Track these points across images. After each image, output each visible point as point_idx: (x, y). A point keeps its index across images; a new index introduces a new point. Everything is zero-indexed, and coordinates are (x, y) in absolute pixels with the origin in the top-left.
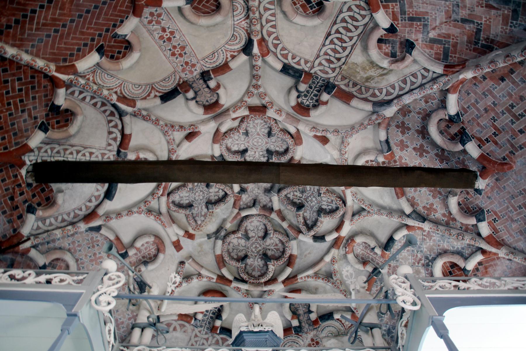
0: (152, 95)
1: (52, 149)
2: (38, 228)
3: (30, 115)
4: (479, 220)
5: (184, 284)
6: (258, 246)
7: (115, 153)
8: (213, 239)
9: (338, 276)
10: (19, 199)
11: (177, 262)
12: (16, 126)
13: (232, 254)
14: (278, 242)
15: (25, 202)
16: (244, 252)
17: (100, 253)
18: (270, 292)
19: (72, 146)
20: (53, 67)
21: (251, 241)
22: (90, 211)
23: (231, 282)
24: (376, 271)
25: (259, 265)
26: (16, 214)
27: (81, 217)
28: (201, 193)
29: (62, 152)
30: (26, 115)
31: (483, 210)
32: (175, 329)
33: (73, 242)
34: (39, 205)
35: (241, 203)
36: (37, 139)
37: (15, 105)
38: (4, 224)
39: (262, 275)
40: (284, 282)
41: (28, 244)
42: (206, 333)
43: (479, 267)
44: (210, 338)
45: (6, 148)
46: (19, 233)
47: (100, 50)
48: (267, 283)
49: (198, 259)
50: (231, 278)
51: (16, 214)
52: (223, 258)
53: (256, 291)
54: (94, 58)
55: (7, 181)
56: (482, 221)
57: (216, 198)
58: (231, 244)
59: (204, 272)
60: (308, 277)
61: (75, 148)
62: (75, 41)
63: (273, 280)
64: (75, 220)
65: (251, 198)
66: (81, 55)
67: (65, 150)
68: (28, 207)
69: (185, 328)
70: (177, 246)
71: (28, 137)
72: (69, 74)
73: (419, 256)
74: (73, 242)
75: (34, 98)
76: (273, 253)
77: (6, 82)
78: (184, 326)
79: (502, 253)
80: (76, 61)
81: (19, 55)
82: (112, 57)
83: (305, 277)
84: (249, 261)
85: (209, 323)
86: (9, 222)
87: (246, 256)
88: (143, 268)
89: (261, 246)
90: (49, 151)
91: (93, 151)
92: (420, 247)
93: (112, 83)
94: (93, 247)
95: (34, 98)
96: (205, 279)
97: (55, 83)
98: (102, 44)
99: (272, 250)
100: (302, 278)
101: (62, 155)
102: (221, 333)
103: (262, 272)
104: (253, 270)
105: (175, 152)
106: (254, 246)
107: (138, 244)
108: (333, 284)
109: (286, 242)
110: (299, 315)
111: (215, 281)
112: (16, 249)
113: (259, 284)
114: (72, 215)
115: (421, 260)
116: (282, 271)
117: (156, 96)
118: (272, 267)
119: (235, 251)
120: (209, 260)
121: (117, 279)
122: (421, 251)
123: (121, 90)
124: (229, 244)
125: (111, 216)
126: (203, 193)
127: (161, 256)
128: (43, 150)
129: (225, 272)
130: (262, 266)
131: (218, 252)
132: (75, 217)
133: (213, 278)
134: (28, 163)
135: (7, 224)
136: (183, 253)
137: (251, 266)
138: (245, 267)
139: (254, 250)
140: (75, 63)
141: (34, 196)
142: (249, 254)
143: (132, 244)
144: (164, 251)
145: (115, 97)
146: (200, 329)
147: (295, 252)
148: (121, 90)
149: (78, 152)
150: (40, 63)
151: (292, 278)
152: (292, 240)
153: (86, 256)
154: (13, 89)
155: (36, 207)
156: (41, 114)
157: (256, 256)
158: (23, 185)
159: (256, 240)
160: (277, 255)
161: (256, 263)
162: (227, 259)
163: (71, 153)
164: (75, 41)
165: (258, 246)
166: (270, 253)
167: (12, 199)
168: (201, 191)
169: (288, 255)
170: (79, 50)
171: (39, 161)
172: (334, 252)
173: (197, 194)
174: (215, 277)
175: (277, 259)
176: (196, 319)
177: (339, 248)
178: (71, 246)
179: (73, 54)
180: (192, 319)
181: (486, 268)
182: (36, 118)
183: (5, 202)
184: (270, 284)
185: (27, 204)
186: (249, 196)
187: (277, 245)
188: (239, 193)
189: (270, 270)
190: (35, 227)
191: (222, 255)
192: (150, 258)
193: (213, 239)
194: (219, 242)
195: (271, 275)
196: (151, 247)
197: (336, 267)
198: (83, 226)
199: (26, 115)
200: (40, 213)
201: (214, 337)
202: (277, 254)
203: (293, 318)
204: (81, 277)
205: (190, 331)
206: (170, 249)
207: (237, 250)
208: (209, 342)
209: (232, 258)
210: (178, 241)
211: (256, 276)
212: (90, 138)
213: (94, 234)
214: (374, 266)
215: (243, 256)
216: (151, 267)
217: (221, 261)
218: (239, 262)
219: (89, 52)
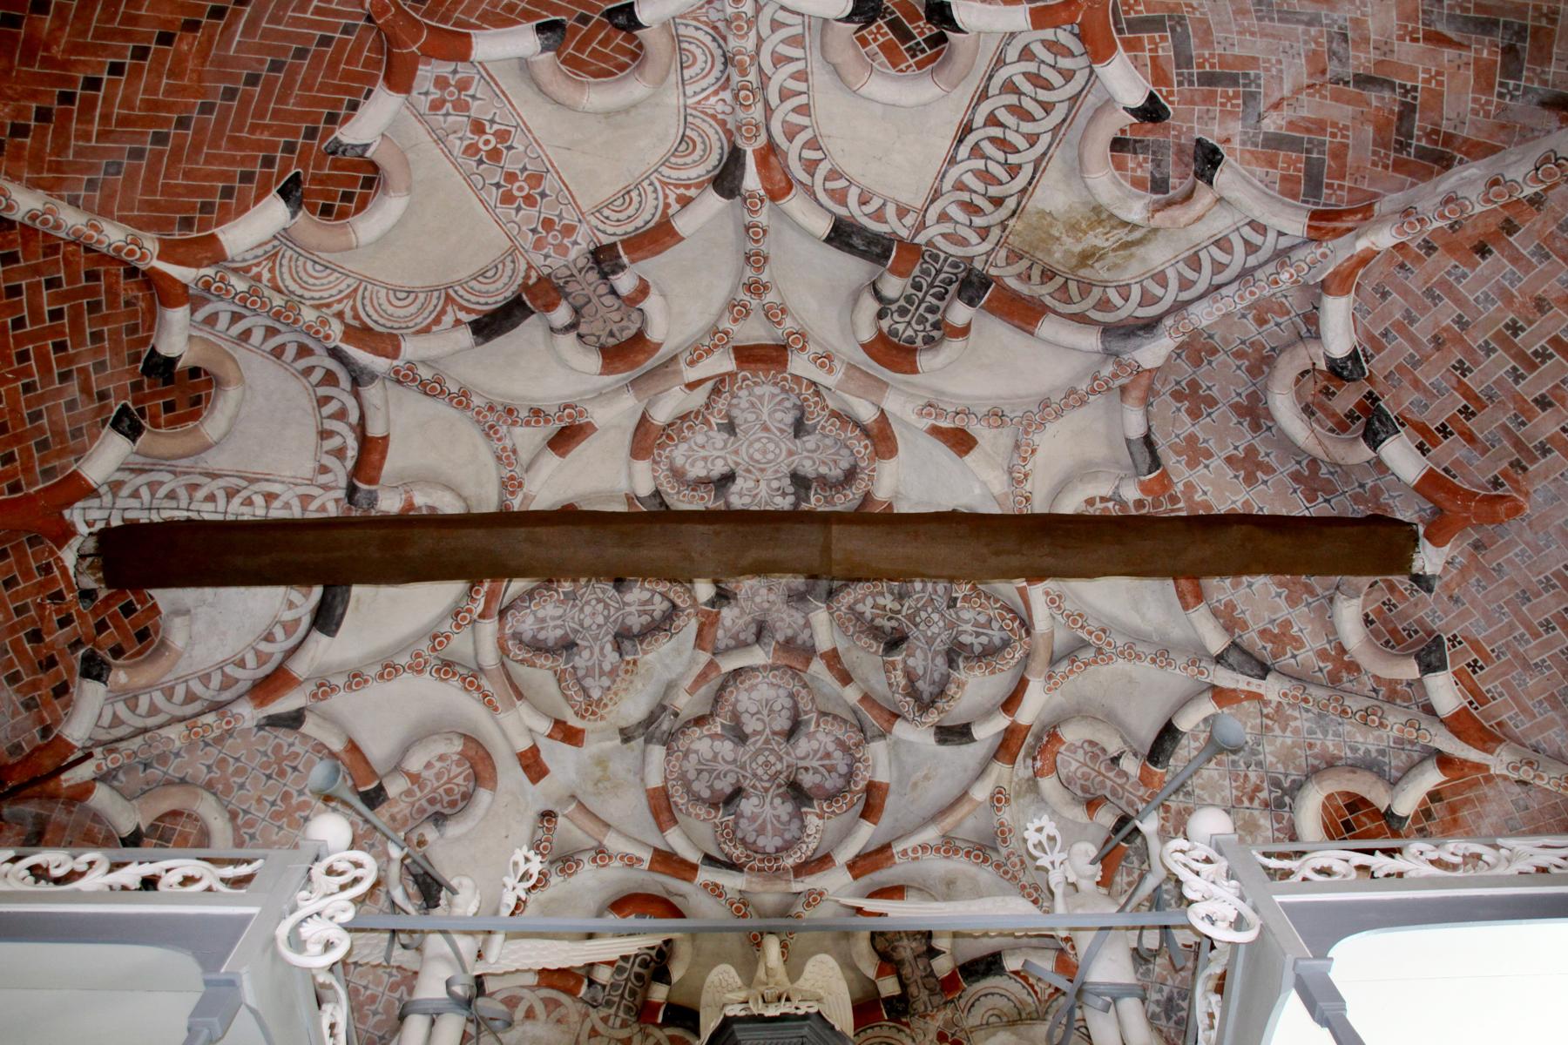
1: (153, 486)
6: (772, 759)
12: (45, 421)
13: (696, 786)
14: (831, 747)
16: (731, 779)
19: (214, 476)
20: (151, 243)
22: (268, 669)
26: (48, 680)
30: (74, 387)
32: (530, 1014)
33: (222, 762)
34: (117, 652)
38: (15, 714)
41: (85, 772)
42: (624, 1025)
49: (593, 804)
50: (694, 857)
51: (48, 680)
52: (668, 797)
54: (272, 214)
59: (613, 843)
61: (221, 482)
64: (226, 696)
65: (748, 618)
66: (234, 204)
68: (85, 659)
69: (562, 1010)
71: (80, 453)
74: (222, 762)
75: (97, 337)
76: (817, 779)
80: (219, 224)
83: (915, 850)
84: (747, 806)
85: (633, 993)
86: (27, 707)
87: (738, 792)
91: (275, 488)
92: (1254, 753)
94: (282, 773)
98: (297, 174)
99: (816, 771)
104: (761, 831)
106: (761, 759)
109: (857, 745)
110: (901, 963)
113: (778, 873)
114: (216, 680)
115: (1258, 789)
116: (846, 833)
117: (458, 322)
119: (705, 775)
122: (1259, 764)
123: (354, 308)
124: (686, 755)
130: (785, 818)
131: (655, 781)
132: (224, 687)
133: (640, 860)
134: (83, 529)
135: (25, 714)
137: (753, 819)
139: (760, 771)
140: (216, 231)
142: (746, 784)
145: (336, 329)
147: (882, 776)
148: (354, 308)
149: (231, 494)
152: (873, 738)
153: (260, 800)
155: (109, 658)
156: (117, 381)
157: (767, 790)
158: (69, 597)
159: (767, 742)
160: (829, 784)
162: (679, 799)
163: (211, 498)
165: (772, 759)
166: (807, 780)
167: (36, 636)
168: (599, 601)
169: (862, 785)
170: (227, 192)
173: (588, 610)
176: (592, 983)
182: (103, 396)
183: (16, 646)
184: (811, 873)
185: (81, 652)
186: (743, 611)
187: (828, 755)
188: (712, 603)
189: (811, 830)
190: (106, 720)
191: (664, 789)
196: (455, 770)
199: (74, 387)
201: (647, 1036)
202: (832, 783)
207: (710, 772)
210: (535, 750)
211: (770, 849)
213: (284, 736)
214: (1119, 812)
215: (728, 790)
219: (258, 199)
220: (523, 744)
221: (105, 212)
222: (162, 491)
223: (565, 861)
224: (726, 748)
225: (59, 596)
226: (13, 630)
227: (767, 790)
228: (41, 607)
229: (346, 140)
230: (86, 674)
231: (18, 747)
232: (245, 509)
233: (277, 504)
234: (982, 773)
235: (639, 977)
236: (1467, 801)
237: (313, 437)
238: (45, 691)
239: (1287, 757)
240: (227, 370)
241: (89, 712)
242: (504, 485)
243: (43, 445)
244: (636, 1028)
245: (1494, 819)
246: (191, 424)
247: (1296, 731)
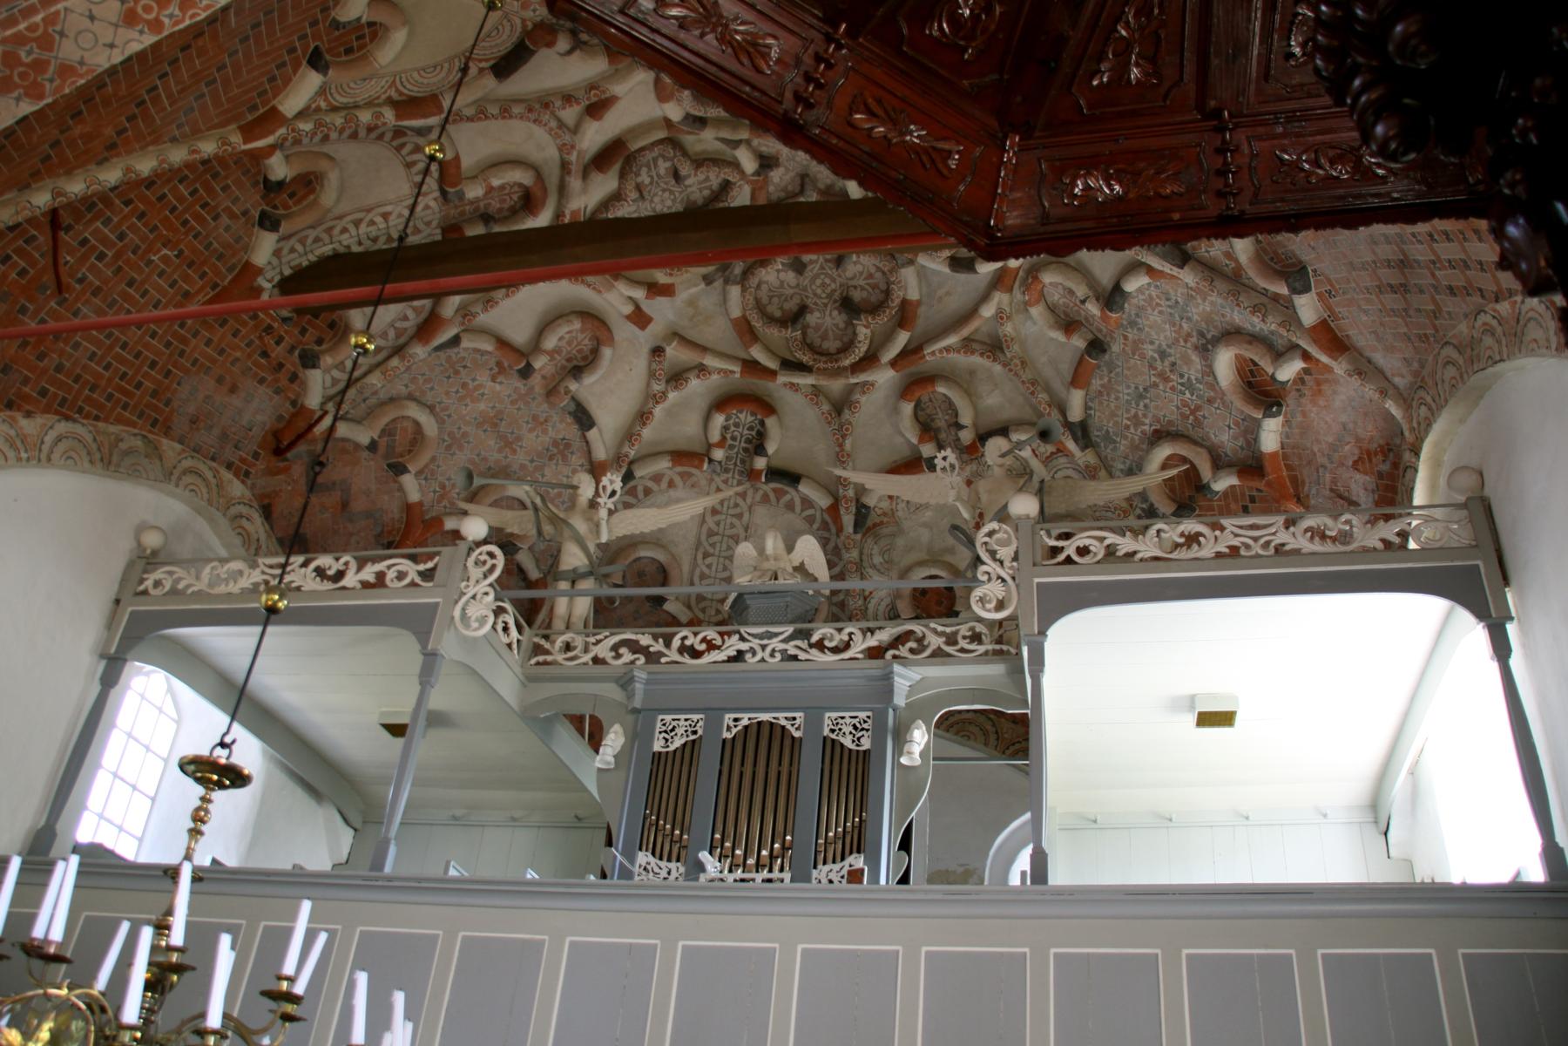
0: (473, 70)
1: (302, 242)
2: (335, 381)
3: (232, 216)
4: (1295, 291)
5: (672, 395)
6: (827, 281)
7: (437, 194)
8: (718, 284)
9: (1016, 347)
10: (278, 352)
11: (645, 351)
12: (215, 245)
13: (770, 309)
14: (873, 270)
15: (292, 350)
16: (796, 300)
17: (474, 380)
18: (866, 387)
19: (340, 218)
20: (236, 139)
21: (808, 273)
22: (424, 315)
23: (772, 374)
24: (1097, 347)
25: (836, 325)
26: (283, 378)
27: (410, 332)
28: (666, 194)
29: (325, 237)
30: (225, 220)
31: (1304, 268)
32: (671, 484)
33: (414, 380)
34: (319, 342)
35: (771, 189)
36: (264, 250)
37: (198, 218)
38: (271, 399)
39: (847, 348)
40: (894, 363)
41: (327, 422)
42: (740, 483)
43: (1306, 378)
44: (750, 493)
45: (215, 286)
46: (303, 406)
47: (317, 61)
48: (857, 368)
49: (692, 334)
50: (772, 364)
51: (283, 378)
52: (748, 323)
53: (836, 385)
54: (310, 82)
55: (244, 331)
56: (1300, 293)
57: (706, 193)
58: (764, 287)
59: (710, 361)
60: (948, 349)
61: (349, 218)
62: (256, 73)
63: (870, 360)
64: (402, 341)
65: (792, 174)
66: (280, 82)
67: (329, 230)
68: (301, 357)
69: (694, 479)
70: (640, 318)
71: (246, 248)
72: (273, 132)
73: (1185, 326)
74: (414, 380)
75: (225, 188)
76: (865, 294)
77: (164, 196)
78: (690, 475)
79: (1340, 367)
80: (275, 97)
81: (163, 161)
82: (348, 51)
83: (941, 351)
84: (812, 319)
85: (743, 462)
86: (277, 393)
87: (803, 310)
88: (573, 386)
89: (834, 280)
90: (299, 248)
91: (389, 208)
92: (1184, 311)
93: (375, 88)
94: (457, 373)
95: (225, 188)
96: (715, 377)
97: (258, 157)
98: (317, 48)
99: (863, 289)
100: (933, 353)
101: (327, 240)
102: (768, 481)
103: (846, 339)
104: (824, 337)
105: (573, 147)
106: (818, 282)
107: (550, 342)
108: (1005, 365)
109: (891, 271)
110: (938, 430)
111: (738, 375)
112: (310, 436)
113: (838, 372)
114: (392, 334)
115: (1189, 335)
116: (888, 337)
117: (481, 70)
118: (864, 332)
119: (775, 300)
120: (717, 331)
121: (490, 562)
122: (1189, 319)
123: (397, 90)
124: (758, 286)
125: (473, 310)
126: (671, 192)
127: (607, 352)
128: (285, 251)
129: (757, 353)
130: (842, 325)
131: (736, 313)
132: (398, 336)
133: (732, 372)
134: (267, 285)
135: (277, 397)
136: (656, 329)
137: (817, 328)
138: (804, 334)
139: (819, 291)
140: (275, 102)
141: (303, 331)
142: (809, 302)
143: (536, 345)
144: (610, 340)
145: (389, 115)
146: (725, 476)
147: (913, 295)
148: (397, 90)
149: (357, 223)
150: (208, 148)
151: (911, 352)
152: (903, 266)
153: (447, 393)
154: (181, 199)
155: (316, 348)
156: (253, 202)
157: (826, 305)
158: (276, 325)
159: (822, 268)
160: (873, 299)
161: (828, 321)
162: (757, 324)
163: (345, 230)
164: (256, 73)
165: (827, 281)
166: (857, 296)
167: (265, 354)
168: (664, 190)
169: (897, 301)
170: (272, 79)
171: (287, 272)
172: (999, 299)
173: (656, 199)
174: (737, 368)
175: (874, 309)
176: (711, 461)
177: (1010, 290)
178: (412, 387)
179: (265, 92)
180: (702, 461)
181: (1318, 383)
182: (245, 213)
183: (256, 364)
184: (863, 370)
185: (297, 353)
186: (787, 170)
187: (871, 276)
188: (757, 173)
189: (861, 337)
190: (328, 383)
191: (744, 317)
192: (585, 358)
193: (718, 284)
194: (735, 292)
195: (864, 348)
196: (581, 336)
197: (1008, 329)
198: (419, 351)
199: (225, 220)
200: (327, 360)
201: (757, 490)
202: (875, 297)
203: (921, 440)
204: (430, 565)
205: (703, 482)
206: (624, 331)
207: (779, 296)
208: (749, 500)
209: (770, 319)
210: (638, 307)
211: (833, 350)
212: (374, 197)
213: (452, 352)
214: (1090, 337)
215: (795, 309)
216: (589, 380)
217: (745, 330)
218: (786, 328)
219: (295, 72)
220: (628, 309)
221: (196, 133)
222: (309, 241)
223: (677, 378)
224: (790, 276)
225: (270, 327)
226: (249, 356)
227: (826, 305)
228: (260, 338)
229: (343, 19)
230: (305, 366)
231: (281, 417)
232: (339, 358)
233: (392, 218)
234: (985, 298)
235: (746, 450)
236: (1327, 381)
237: (401, 170)
238: (284, 382)
239: (1208, 320)
240: (323, 165)
241: (317, 386)
242: (560, 150)
243: (221, 257)
244: (747, 485)
245: (1343, 397)
246: (312, 197)
247: (1212, 303)
